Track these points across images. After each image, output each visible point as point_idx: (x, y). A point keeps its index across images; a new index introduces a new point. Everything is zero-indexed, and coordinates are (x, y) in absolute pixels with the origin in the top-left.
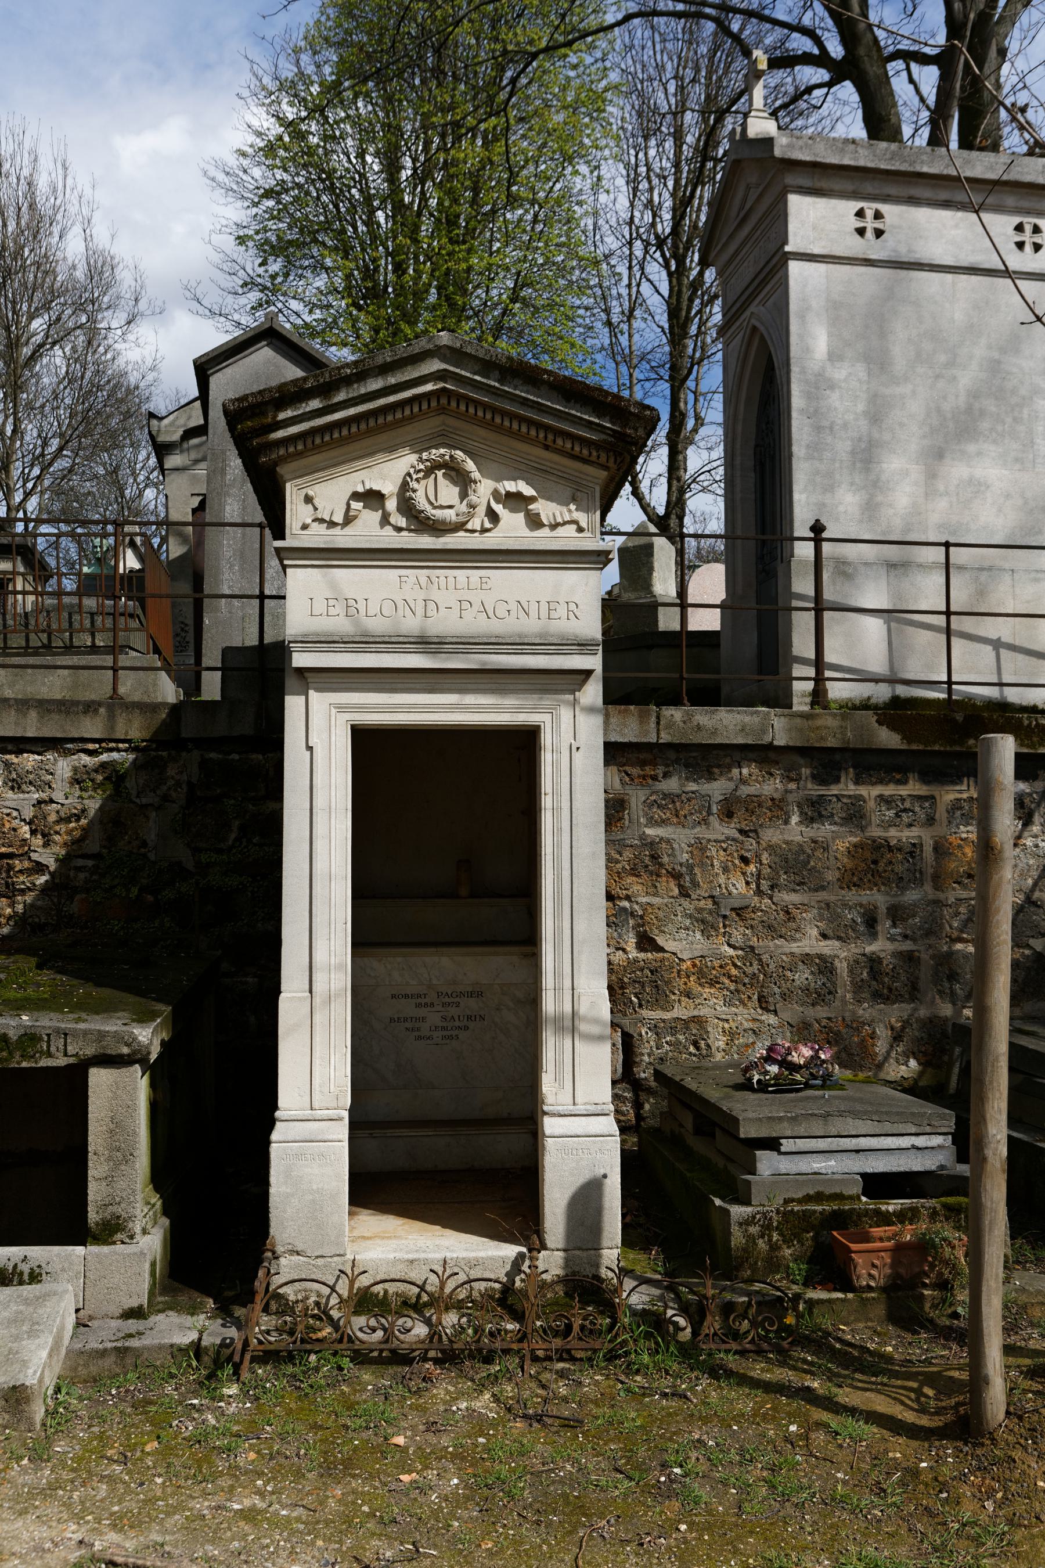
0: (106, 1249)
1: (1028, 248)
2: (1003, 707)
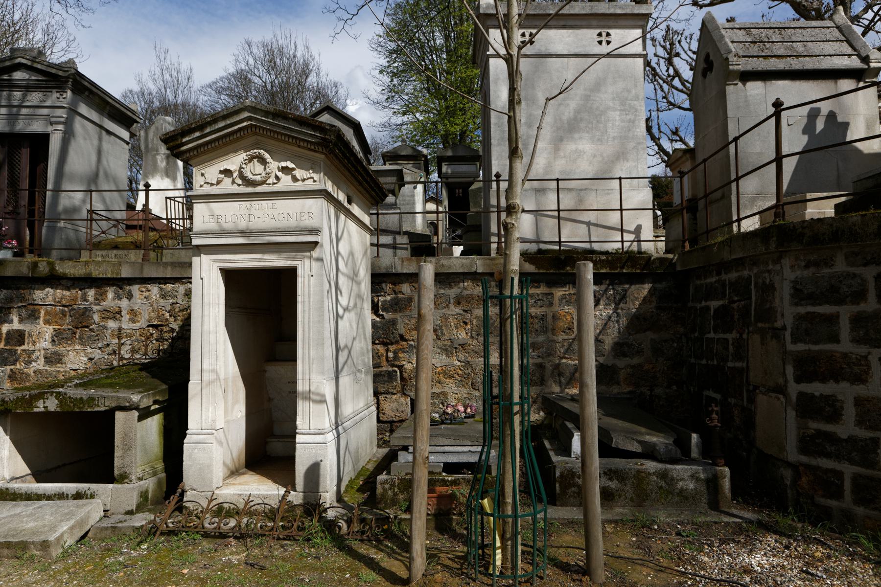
0: (120, 486)
1: (604, 43)
2: (592, 252)
